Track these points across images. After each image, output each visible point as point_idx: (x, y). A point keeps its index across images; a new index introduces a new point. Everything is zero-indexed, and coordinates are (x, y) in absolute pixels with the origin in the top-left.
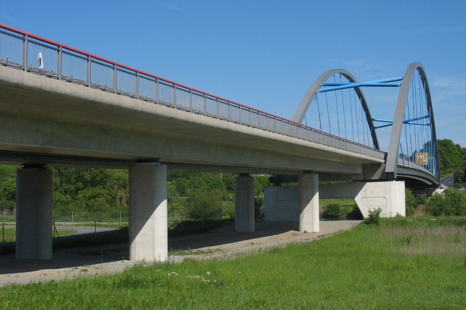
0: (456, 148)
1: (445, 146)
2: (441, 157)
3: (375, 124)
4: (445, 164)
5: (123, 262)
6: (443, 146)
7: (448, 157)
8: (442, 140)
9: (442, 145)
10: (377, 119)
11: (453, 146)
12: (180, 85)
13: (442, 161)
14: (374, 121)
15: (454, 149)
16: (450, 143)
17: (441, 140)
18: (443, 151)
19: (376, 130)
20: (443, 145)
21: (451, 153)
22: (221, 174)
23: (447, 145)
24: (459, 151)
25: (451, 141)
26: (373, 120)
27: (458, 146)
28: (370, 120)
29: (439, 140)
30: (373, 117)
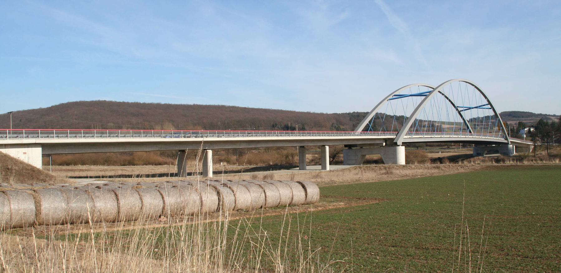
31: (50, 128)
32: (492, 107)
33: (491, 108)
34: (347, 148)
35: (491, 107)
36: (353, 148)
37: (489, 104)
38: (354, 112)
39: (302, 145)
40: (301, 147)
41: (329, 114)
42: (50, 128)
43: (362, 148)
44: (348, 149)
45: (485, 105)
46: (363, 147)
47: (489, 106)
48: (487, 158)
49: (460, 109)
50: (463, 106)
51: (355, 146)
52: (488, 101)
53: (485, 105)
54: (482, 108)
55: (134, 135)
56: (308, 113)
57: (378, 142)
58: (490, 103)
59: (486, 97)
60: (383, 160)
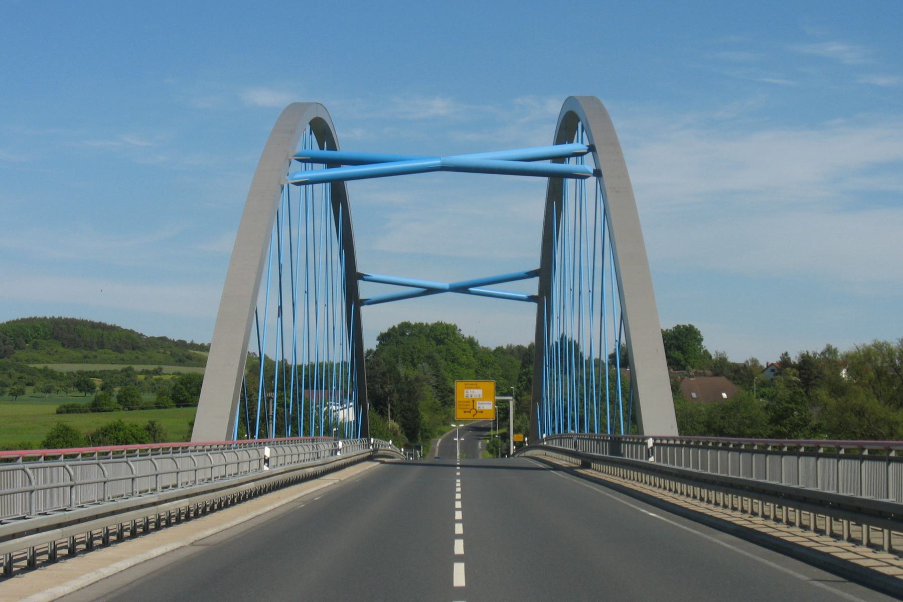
0: (467, 347)
1: (440, 342)
2: (433, 375)
3: (365, 290)
4: (443, 395)
5: (888, 572)
6: (433, 343)
7: (451, 376)
8: (430, 323)
9: (431, 339)
10: (375, 276)
11: (460, 341)
12: (593, 265)
13: (437, 387)
14: (364, 280)
15: (464, 350)
16: (454, 333)
17: (427, 325)
18: (437, 356)
19: (364, 309)
20: (435, 339)
21: (458, 363)
22: (668, 449)
23: (446, 340)
24: (474, 356)
25: (455, 327)
26: (361, 277)
27: (471, 342)
28: (352, 278)
29: (422, 324)
30: (361, 267)
39: (251, 448)
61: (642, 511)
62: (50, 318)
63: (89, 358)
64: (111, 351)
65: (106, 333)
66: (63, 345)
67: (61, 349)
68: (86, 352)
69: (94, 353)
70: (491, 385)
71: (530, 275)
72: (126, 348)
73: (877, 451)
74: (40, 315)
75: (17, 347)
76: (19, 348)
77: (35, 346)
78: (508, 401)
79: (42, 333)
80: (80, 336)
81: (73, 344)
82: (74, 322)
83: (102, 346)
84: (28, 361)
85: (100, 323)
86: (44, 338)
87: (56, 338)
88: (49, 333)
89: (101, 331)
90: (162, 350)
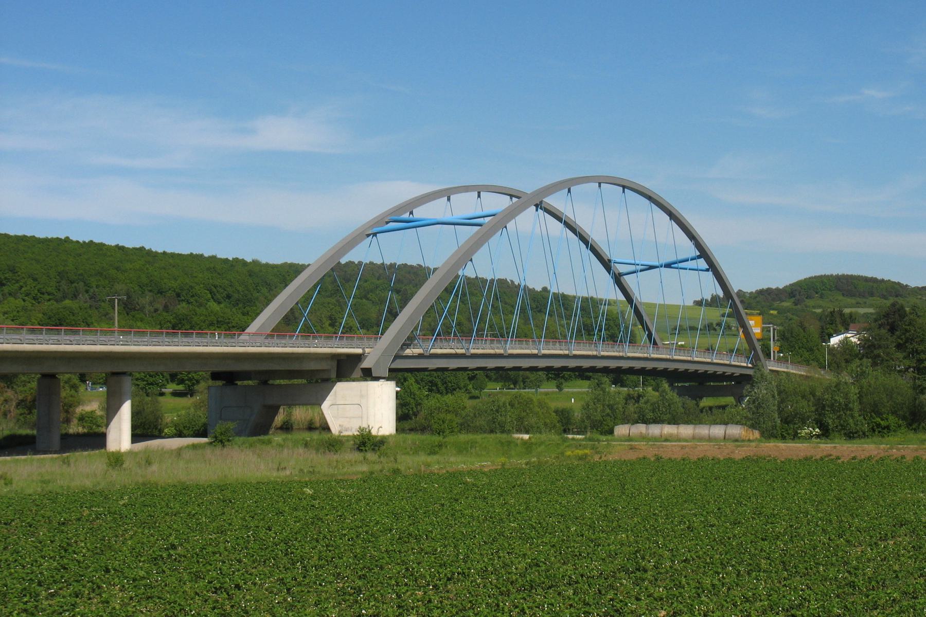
29: (353, 263)
31: (341, 321)
32: (713, 267)
33: (707, 270)
34: (219, 383)
35: (708, 267)
36: (239, 383)
37: (699, 257)
38: (350, 261)
39: (47, 369)
40: (44, 376)
41: (267, 265)
42: (769, 342)
43: (265, 383)
44: (223, 385)
45: (687, 260)
46: (271, 382)
47: (702, 264)
48: (169, 418)
49: (622, 269)
50: (696, 268)
51: (246, 375)
52: (699, 245)
53: (687, 260)
54: (677, 268)
55: (9, 331)
56: (195, 258)
57: (313, 366)
58: (703, 253)
59: (691, 236)
60: (327, 423)
61: (694, 383)
62: (836, 275)
63: (860, 304)
64: (878, 298)
65: (875, 285)
66: (843, 295)
67: (841, 298)
68: (859, 300)
69: (864, 300)
70: (759, 318)
71: (624, 191)
72: (891, 296)
73: (323, 371)
74: (828, 273)
75: (809, 297)
76: (810, 298)
77: (822, 297)
78: (769, 327)
79: (829, 287)
80: (856, 288)
81: (850, 294)
82: (852, 277)
83: (872, 294)
84: (814, 307)
85: (872, 277)
86: (830, 290)
87: (839, 290)
88: (834, 286)
89: (871, 284)
90: (920, 297)
